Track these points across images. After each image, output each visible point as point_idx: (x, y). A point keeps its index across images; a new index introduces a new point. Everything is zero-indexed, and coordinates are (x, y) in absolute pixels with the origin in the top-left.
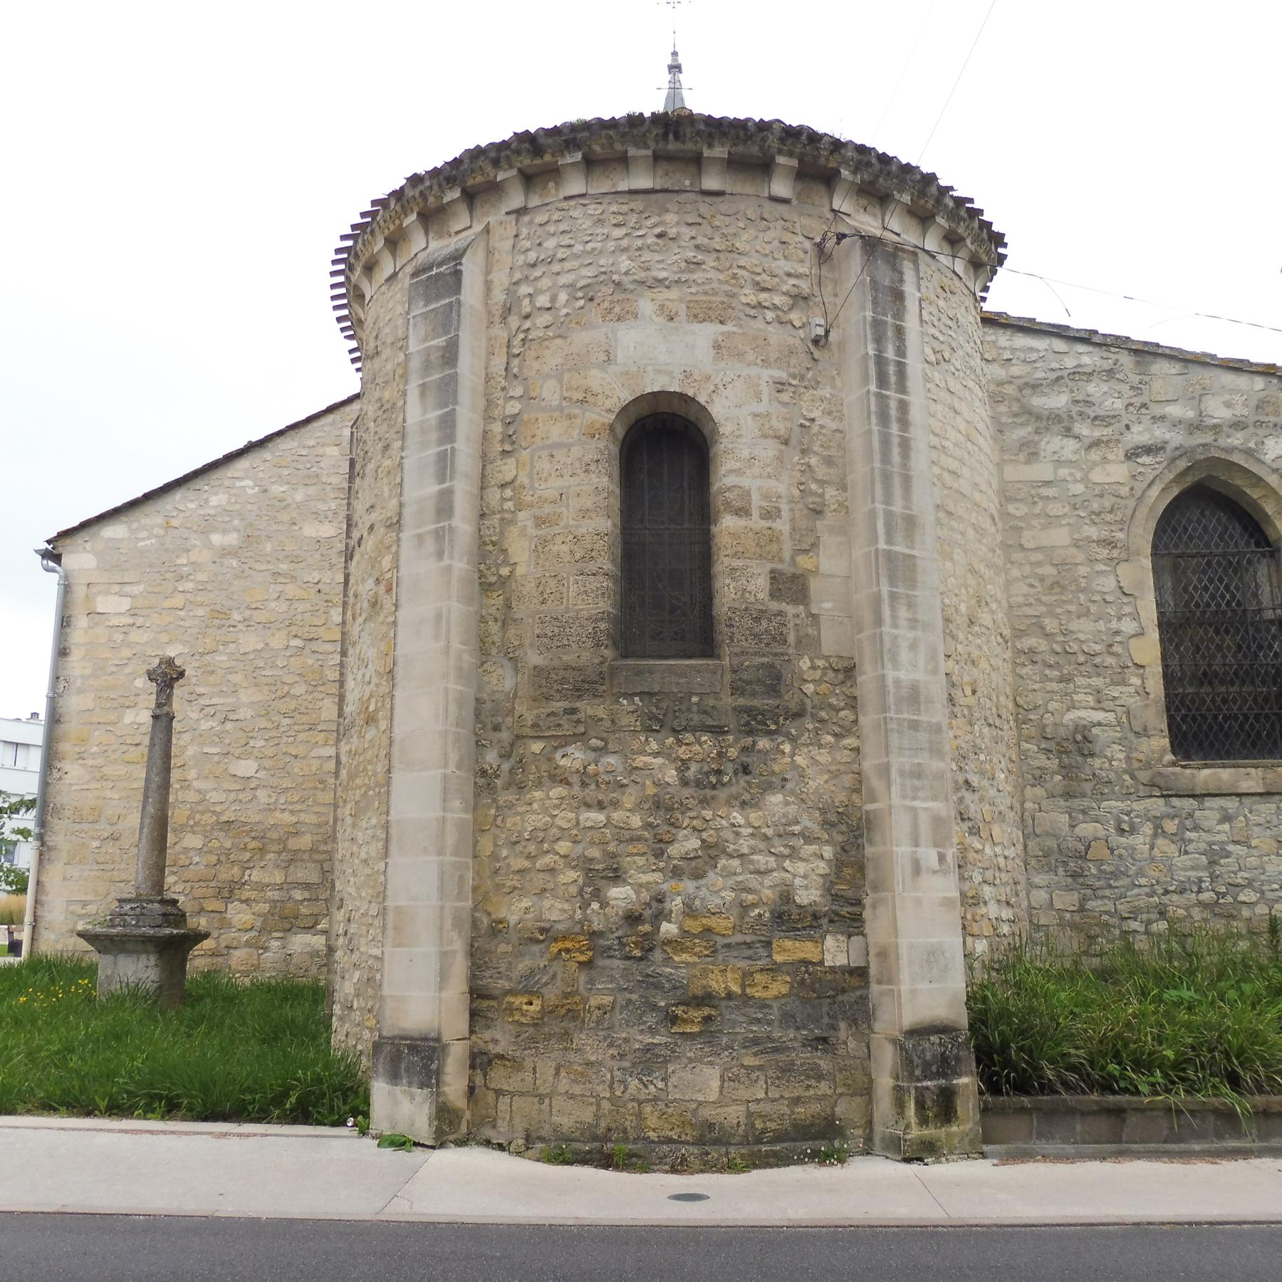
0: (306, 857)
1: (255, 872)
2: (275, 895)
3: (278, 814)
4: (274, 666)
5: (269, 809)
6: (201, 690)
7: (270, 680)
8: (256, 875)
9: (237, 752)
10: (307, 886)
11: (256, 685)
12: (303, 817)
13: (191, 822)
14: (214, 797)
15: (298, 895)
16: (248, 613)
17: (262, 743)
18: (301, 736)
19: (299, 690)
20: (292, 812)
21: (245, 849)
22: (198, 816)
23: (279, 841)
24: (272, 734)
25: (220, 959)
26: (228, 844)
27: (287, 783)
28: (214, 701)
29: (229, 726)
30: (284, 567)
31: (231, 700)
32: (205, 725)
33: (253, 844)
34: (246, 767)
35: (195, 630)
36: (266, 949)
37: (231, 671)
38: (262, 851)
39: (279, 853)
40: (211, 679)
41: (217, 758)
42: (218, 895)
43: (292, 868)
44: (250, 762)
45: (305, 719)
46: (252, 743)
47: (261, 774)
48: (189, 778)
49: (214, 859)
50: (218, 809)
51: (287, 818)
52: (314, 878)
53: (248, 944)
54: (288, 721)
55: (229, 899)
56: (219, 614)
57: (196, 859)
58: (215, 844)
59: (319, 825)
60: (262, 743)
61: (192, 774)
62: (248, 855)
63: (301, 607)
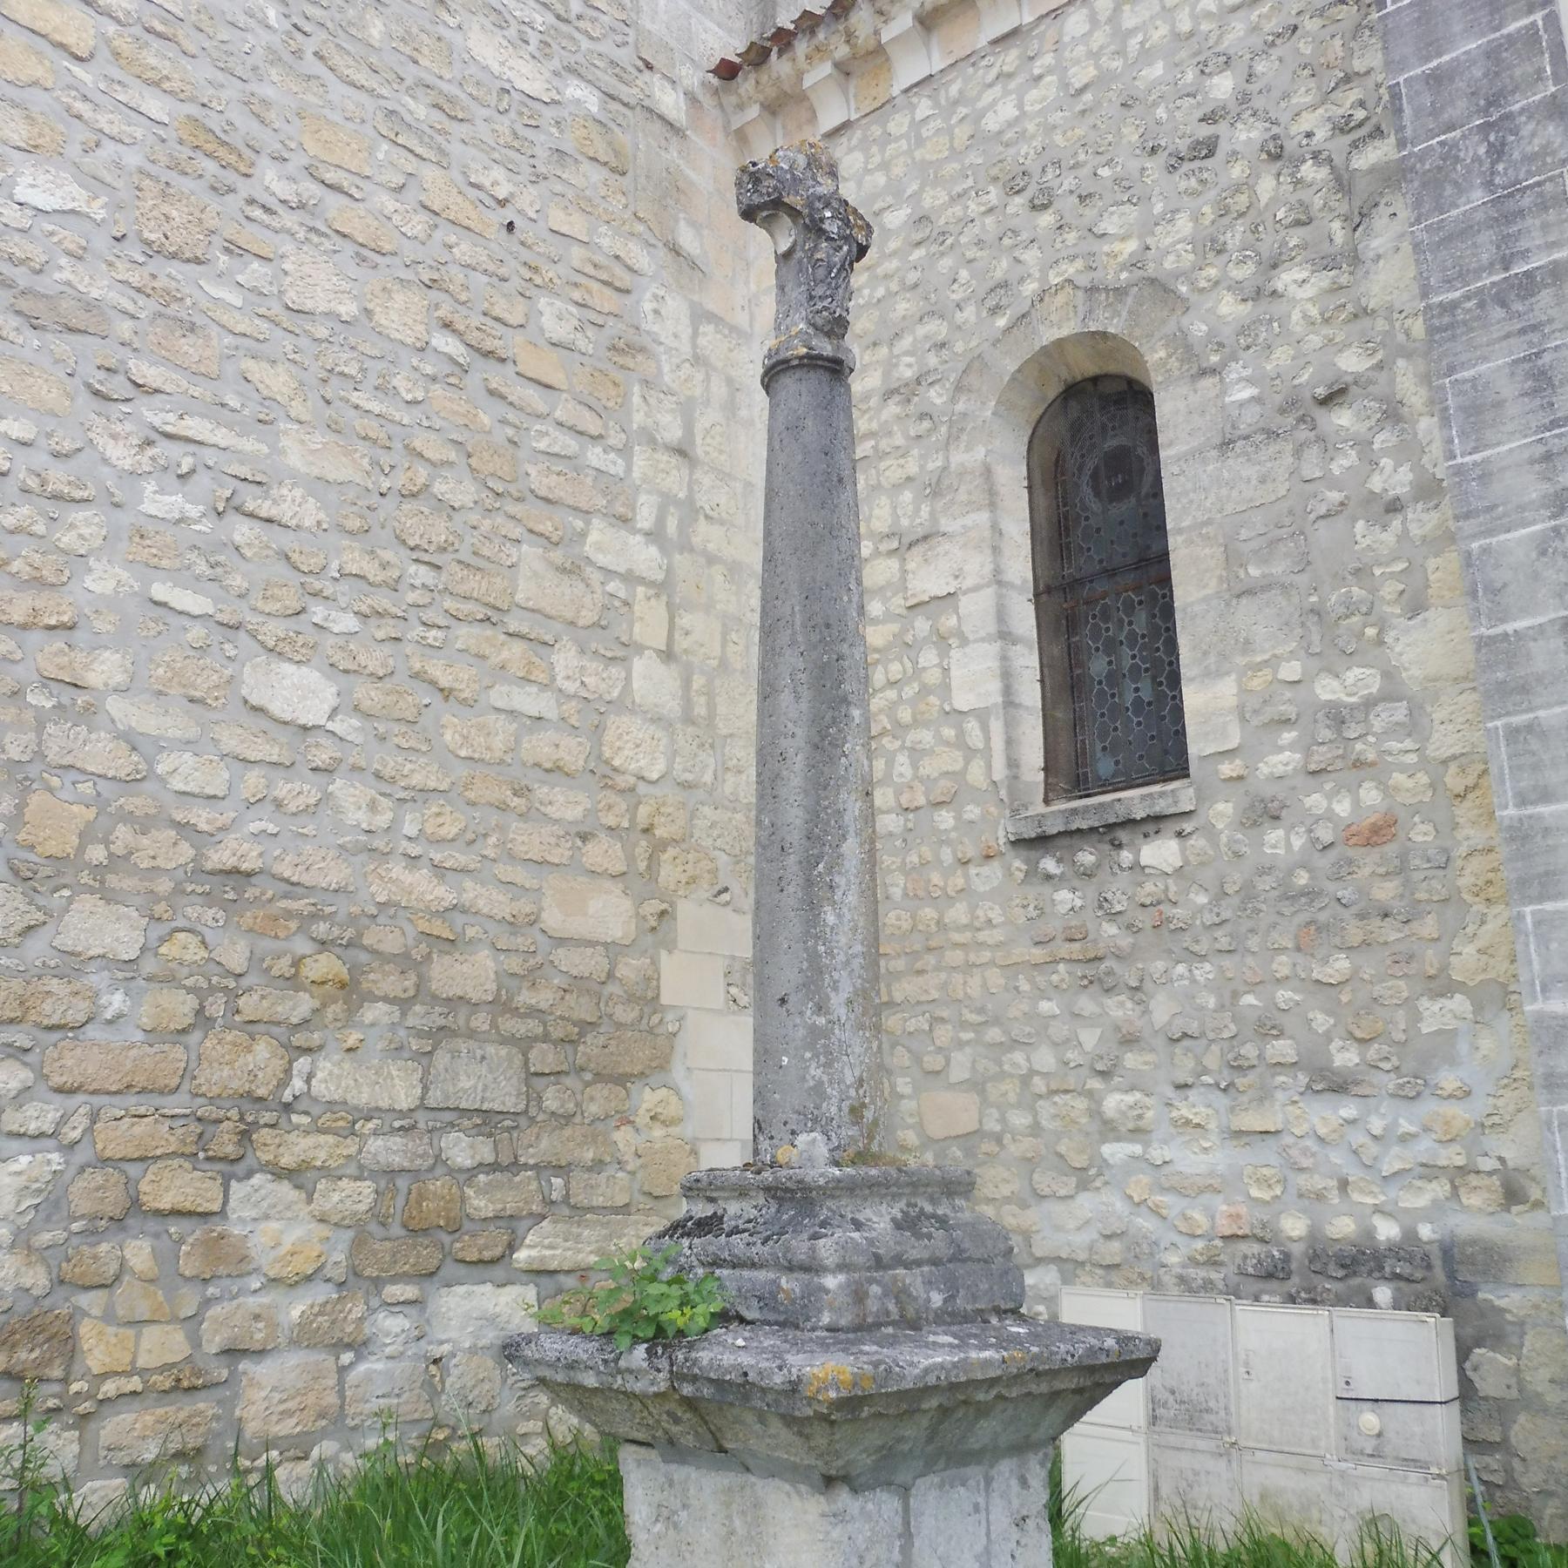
0: (481, 1021)
1: (325, 1067)
2: (386, 1149)
3: (397, 870)
4: (384, 389)
5: (371, 849)
6: (149, 373)
7: (372, 428)
8: (328, 1077)
9: (273, 630)
10: (486, 1121)
11: (333, 428)
12: (472, 891)
13: (97, 854)
14: (183, 771)
15: (462, 1150)
16: (311, 189)
17: (348, 623)
18: (465, 635)
19: (458, 489)
20: (438, 869)
21: (293, 981)
22: (123, 833)
23: (404, 962)
24: (383, 601)
25: (204, 1405)
26: (235, 955)
27: (422, 774)
28: (194, 426)
29: (243, 531)
30: (419, 109)
31: (248, 445)
32: (159, 502)
33: (324, 966)
34: (300, 692)
35: (133, 159)
36: (361, 1347)
37: (255, 347)
38: (350, 991)
39: (404, 1004)
40: (188, 347)
41: (196, 633)
42: (198, 1153)
43: (442, 1059)
44: (310, 676)
45: (474, 584)
46: (318, 612)
47: (345, 725)
48: (93, 678)
49: (181, 1006)
50: (202, 817)
51: (441, 894)
52: (505, 1095)
53: (304, 1337)
54: (423, 575)
55: (231, 1168)
56: (215, 149)
57: (116, 1002)
58: (185, 948)
59: (512, 925)
60: (348, 623)
61: (105, 669)
62: (303, 1005)
63: (464, 250)
